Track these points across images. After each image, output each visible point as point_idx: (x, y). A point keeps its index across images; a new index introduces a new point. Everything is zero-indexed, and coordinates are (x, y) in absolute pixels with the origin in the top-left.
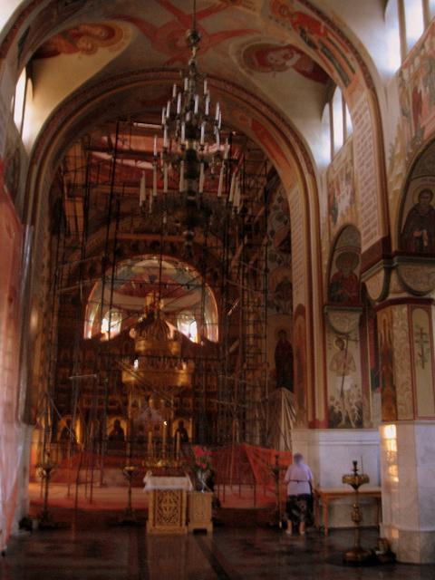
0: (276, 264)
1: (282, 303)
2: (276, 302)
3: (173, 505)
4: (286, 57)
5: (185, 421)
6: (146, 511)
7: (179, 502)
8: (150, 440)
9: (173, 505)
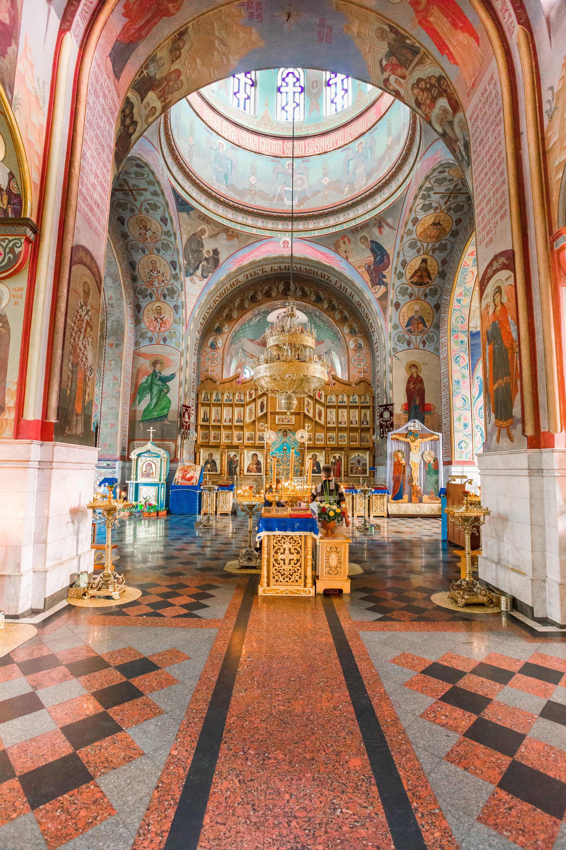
0: (407, 297)
1: (413, 338)
2: (407, 336)
3: (295, 557)
5: (317, 454)
6: (334, 538)
7: (272, 560)
9: (295, 557)
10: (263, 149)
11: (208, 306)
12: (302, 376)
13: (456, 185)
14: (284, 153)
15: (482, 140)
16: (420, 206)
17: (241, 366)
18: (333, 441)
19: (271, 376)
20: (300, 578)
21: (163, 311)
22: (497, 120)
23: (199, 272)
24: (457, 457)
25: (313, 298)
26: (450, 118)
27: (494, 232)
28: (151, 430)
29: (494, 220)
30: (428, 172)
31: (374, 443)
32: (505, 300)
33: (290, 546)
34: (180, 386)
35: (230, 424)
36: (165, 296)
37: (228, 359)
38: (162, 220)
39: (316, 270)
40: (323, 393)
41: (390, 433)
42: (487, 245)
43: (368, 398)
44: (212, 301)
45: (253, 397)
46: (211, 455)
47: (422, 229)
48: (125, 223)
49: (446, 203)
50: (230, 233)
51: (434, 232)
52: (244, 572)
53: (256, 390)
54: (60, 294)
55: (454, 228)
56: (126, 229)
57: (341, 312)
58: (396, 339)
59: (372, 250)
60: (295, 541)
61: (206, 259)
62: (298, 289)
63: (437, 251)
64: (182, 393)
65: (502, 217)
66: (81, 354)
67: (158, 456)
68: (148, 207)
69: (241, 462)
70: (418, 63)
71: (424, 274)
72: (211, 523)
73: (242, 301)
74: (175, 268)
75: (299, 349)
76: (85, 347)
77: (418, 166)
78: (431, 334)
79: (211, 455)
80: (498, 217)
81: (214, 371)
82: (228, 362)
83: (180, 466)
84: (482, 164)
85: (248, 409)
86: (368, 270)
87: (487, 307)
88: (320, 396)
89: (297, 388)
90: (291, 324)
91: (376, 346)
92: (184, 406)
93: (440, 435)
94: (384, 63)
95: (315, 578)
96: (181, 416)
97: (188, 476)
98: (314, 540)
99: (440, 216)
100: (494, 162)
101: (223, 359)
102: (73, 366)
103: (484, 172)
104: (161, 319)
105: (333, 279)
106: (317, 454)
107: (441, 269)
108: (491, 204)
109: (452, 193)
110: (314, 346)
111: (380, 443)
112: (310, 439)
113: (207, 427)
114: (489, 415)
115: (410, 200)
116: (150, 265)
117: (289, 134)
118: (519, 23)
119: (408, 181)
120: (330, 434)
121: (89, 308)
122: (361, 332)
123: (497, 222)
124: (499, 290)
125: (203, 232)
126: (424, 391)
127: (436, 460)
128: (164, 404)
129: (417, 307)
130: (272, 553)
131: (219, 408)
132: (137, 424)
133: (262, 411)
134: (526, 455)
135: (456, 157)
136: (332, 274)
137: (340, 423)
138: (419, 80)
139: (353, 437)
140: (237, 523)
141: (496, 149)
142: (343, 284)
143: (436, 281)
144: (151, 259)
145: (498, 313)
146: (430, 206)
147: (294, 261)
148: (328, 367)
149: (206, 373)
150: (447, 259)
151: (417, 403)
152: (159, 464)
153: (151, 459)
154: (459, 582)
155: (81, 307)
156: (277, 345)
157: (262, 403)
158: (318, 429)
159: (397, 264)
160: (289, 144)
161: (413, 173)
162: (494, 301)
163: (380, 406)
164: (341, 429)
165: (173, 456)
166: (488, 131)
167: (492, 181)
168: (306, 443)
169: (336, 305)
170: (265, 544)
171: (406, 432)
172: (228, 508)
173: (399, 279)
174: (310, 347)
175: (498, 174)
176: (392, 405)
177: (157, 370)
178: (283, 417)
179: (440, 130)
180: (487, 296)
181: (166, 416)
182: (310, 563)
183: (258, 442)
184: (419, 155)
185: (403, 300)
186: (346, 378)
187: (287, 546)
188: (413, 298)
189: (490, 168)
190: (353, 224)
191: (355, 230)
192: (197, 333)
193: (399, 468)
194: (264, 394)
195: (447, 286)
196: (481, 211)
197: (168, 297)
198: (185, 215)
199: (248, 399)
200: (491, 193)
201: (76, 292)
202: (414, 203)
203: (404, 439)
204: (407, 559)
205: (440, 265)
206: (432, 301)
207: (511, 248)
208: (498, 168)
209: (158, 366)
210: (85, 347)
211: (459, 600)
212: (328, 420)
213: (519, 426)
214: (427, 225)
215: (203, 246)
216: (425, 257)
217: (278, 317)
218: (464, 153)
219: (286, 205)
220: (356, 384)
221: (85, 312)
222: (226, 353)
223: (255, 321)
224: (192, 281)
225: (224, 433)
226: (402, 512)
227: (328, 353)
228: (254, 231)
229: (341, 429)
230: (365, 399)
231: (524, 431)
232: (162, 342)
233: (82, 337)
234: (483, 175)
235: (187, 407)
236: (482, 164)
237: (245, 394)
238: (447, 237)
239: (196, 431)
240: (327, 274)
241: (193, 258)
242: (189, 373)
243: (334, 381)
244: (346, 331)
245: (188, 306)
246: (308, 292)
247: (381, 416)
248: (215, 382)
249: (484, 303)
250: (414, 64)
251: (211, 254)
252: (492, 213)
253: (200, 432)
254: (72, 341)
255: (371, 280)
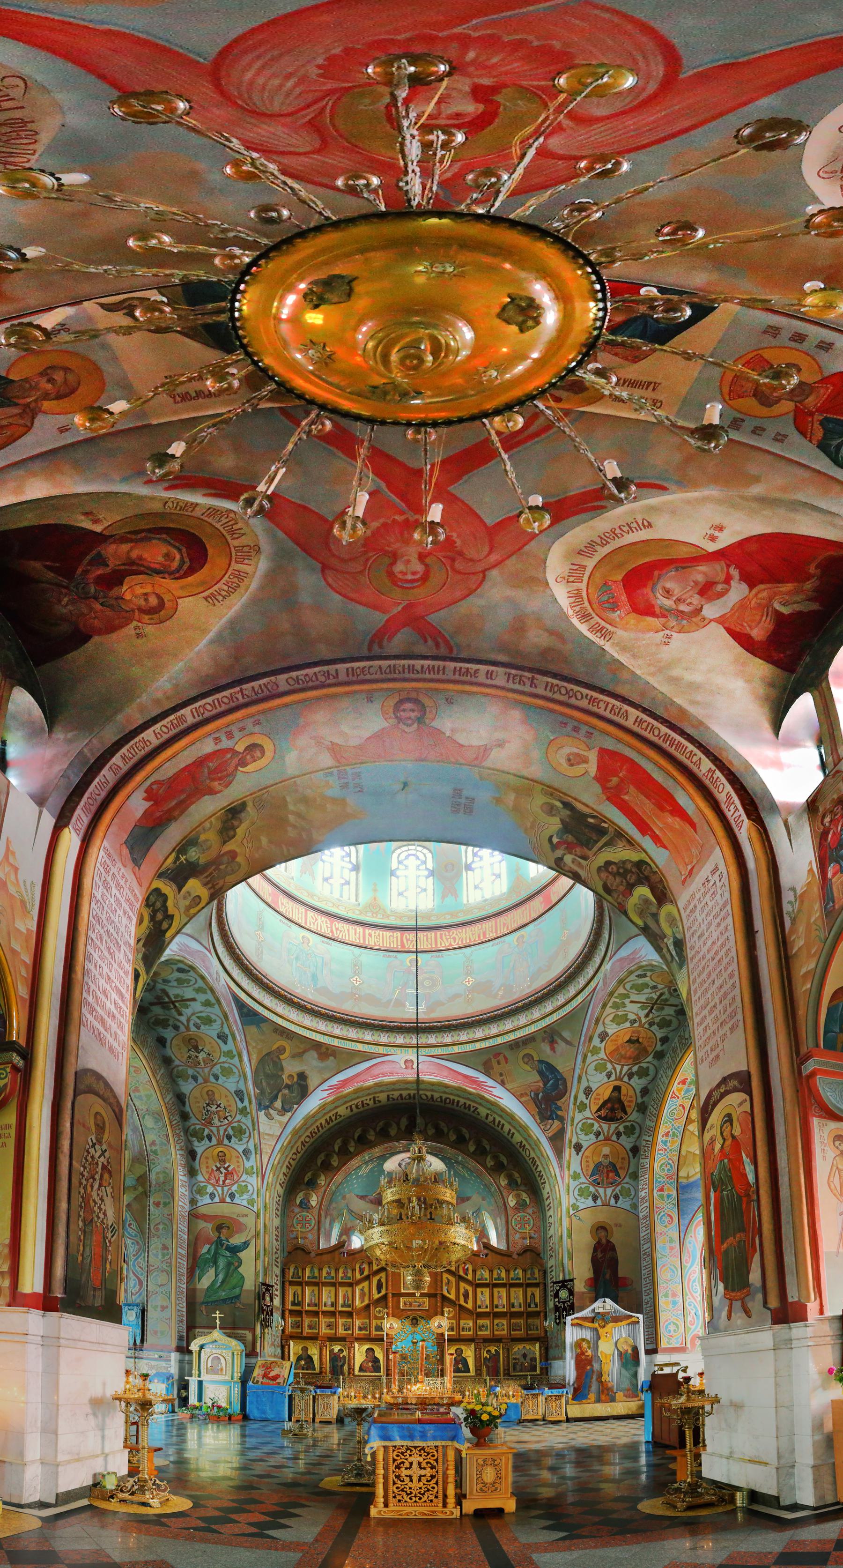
0: (592, 1137)
2: (592, 1189)
3: (428, 1472)
4: (706, 590)
5: (463, 1347)
6: (490, 1448)
7: (392, 1477)
8: (501, 450)
9: (404, 1472)
10: (371, 942)
11: (294, 1150)
12: (437, 1242)
13: (661, 994)
14: (403, 945)
15: (702, 934)
16: (611, 1017)
17: (346, 1232)
18: (486, 1329)
19: (390, 1244)
20: (436, 1497)
21: (228, 1157)
22: (723, 913)
23: (278, 1104)
24: (664, 1343)
25: (453, 1137)
26: (654, 909)
27: (721, 1047)
28: (218, 1314)
29: (722, 1032)
30: (622, 974)
31: (546, 1332)
32: (737, 1132)
33: (421, 1459)
34: (257, 1257)
35: (333, 1309)
36: (229, 1138)
37: (328, 1221)
38: (219, 1037)
39: (457, 1099)
40: (469, 1267)
41: (569, 1318)
42: (711, 1064)
43: (536, 1271)
44: (299, 1144)
45: (366, 1273)
46: (305, 1349)
47: (614, 1047)
48: (168, 1044)
49: (647, 1016)
50: (323, 1050)
51: (630, 1050)
52: (348, 1489)
53: (370, 1264)
54: (61, 1129)
55: (659, 1048)
56: (168, 1052)
57: (495, 1158)
58: (576, 1192)
59: (541, 1073)
60: (428, 1454)
61: (288, 1087)
62: (429, 1126)
63: (636, 1077)
64: (260, 1267)
65: (732, 1029)
66: (96, 1209)
67: (228, 1347)
68: (199, 1021)
69: (351, 1358)
70: (606, 844)
71: (616, 1106)
72: (305, 1431)
73: (345, 1144)
74: (242, 1101)
75: (431, 1205)
76: (102, 1200)
77: (607, 967)
78: (627, 1186)
79: (305, 1349)
80: (727, 1028)
81: (307, 1238)
82: (327, 1225)
83: (260, 1361)
84: (703, 963)
85: (358, 1289)
86: (535, 1100)
87: (712, 1141)
88: (466, 1271)
89: (430, 1260)
90: (418, 1171)
91: (547, 1203)
92: (264, 1284)
93: (641, 1316)
94: (555, 840)
95: (460, 1498)
96: (260, 1297)
97: (272, 1374)
98: (458, 1452)
99: (638, 1032)
100: (720, 962)
101: (319, 1222)
102: (85, 1225)
103: (707, 971)
104: (226, 1169)
105: (483, 1111)
106: (463, 1347)
107: (640, 1100)
108: (717, 1012)
109: (655, 1003)
110: (454, 1202)
111: (555, 1331)
112: (451, 1329)
113: (299, 1313)
114: (716, 1285)
115: (594, 1010)
116: (206, 1097)
117: (412, 923)
118: (749, 818)
119: (593, 984)
120: (481, 1322)
121: (104, 1147)
122: (526, 1185)
123: (725, 1035)
124: (729, 1119)
125: (281, 1050)
126: (617, 1261)
127: (635, 1350)
128: (234, 1281)
129: (606, 1150)
130: (392, 1468)
131: (316, 1288)
132: (198, 1307)
133: (379, 1292)
134: (770, 1332)
135: (663, 957)
136: (480, 1104)
137: (497, 1307)
138: (608, 863)
139: (516, 1324)
140: (343, 1433)
141: (722, 946)
142: (498, 1119)
143: (634, 1116)
144: (206, 1089)
145: (727, 1149)
146: (624, 1018)
147: (421, 1086)
148: (476, 1230)
149: (295, 1242)
150: (650, 1087)
151: (608, 1276)
152: (229, 1359)
153: (219, 1351)
154: (676, 1485)
155: (94, 1145)
156: (398, 1201)
157: (379, 1281)
158: (463, 1315)
159: (578, 1092)
160: (411, 936)
161: (600, 975)
162: (722, 1134)
163: (555, 1283)
164: (497, 1315)
165: (250, 1348)
166: (710, 924)
167: (717, 983)
168: (446, 1333)
169: (488, 1147)
170: (380, 1456)
171: (592, 1315)
172: (333, 1414)
173: (580, 1111)
174: (449, 1203)
175: (725, 975)
176: (572, 1280)
177: (223, 1237)
178: (410, 1299)
179: (640, 923)
180: (712, 1126)
181: (238, 1297)
182: (451, 1479)
183: (374, 1333)
184: (609, 954)
185: (587, 1140)
186: (503, 1247)
187: (415, 1459)
188: (601, 1137)
189: (714, 969)
190: (512, 1037)
191: (515, 1045)
192: (278, 1187)
193: (583, 1363)
194: (383, 1269)
195: (648, 1123)
196: (703, 1020)
197: (233, 1139)
198: (253, 1029)
199: (358, 1276)
200: (716, 999)
201: (84, 1126)
202: (602, 1013)
203: (591, 1325)
204: (596, 1467)
205: (639, 1094)
206: (627, 1142)
207: (745, 1068)
208: (726, 968)
209: (224, 1231)
210: (102, 1200)
211: (679, 1505)
212: (479, 1303)
213: (760, 1296)
214: (620, 1042)
215: (282, 1069)
216: (618, 1083)
217: (400, 1165)
218: (674, 953)
219: (408, 1013)
220: (519, 1254)
221: (99, 1153)
222: (323, 1214)
223: (365, 1170)
224: (269, 1117)
225: (323, 1321)
226: (587, 1415)
227: (478, 1212)
228: (360, 1047)
229: (497, 1315)
230: (533, 1273)
231: (765, 1303)
232: (228, 1200)
233: (96, 1186)
234: (704, 976)
235: (268, 1287)
236: (703, 963)
237: (354, 1270)
238: (650, 1059)
239: (283, 1317)
240: (473, 1104)
241: (268, 1084)
242: (270, 1241)
243: (486, 1251)
244: (503, 1182)
245: (264, 1150)
246: (446, 1130)
247: (556, 1295)
248: (310, 1253)
249: (707, 1137)
250: (600, 844)
251: (295, 1079)
252: (719, 1023)
253: (290, 1320)
254: (82, 1191)
255: (540, 1113)
